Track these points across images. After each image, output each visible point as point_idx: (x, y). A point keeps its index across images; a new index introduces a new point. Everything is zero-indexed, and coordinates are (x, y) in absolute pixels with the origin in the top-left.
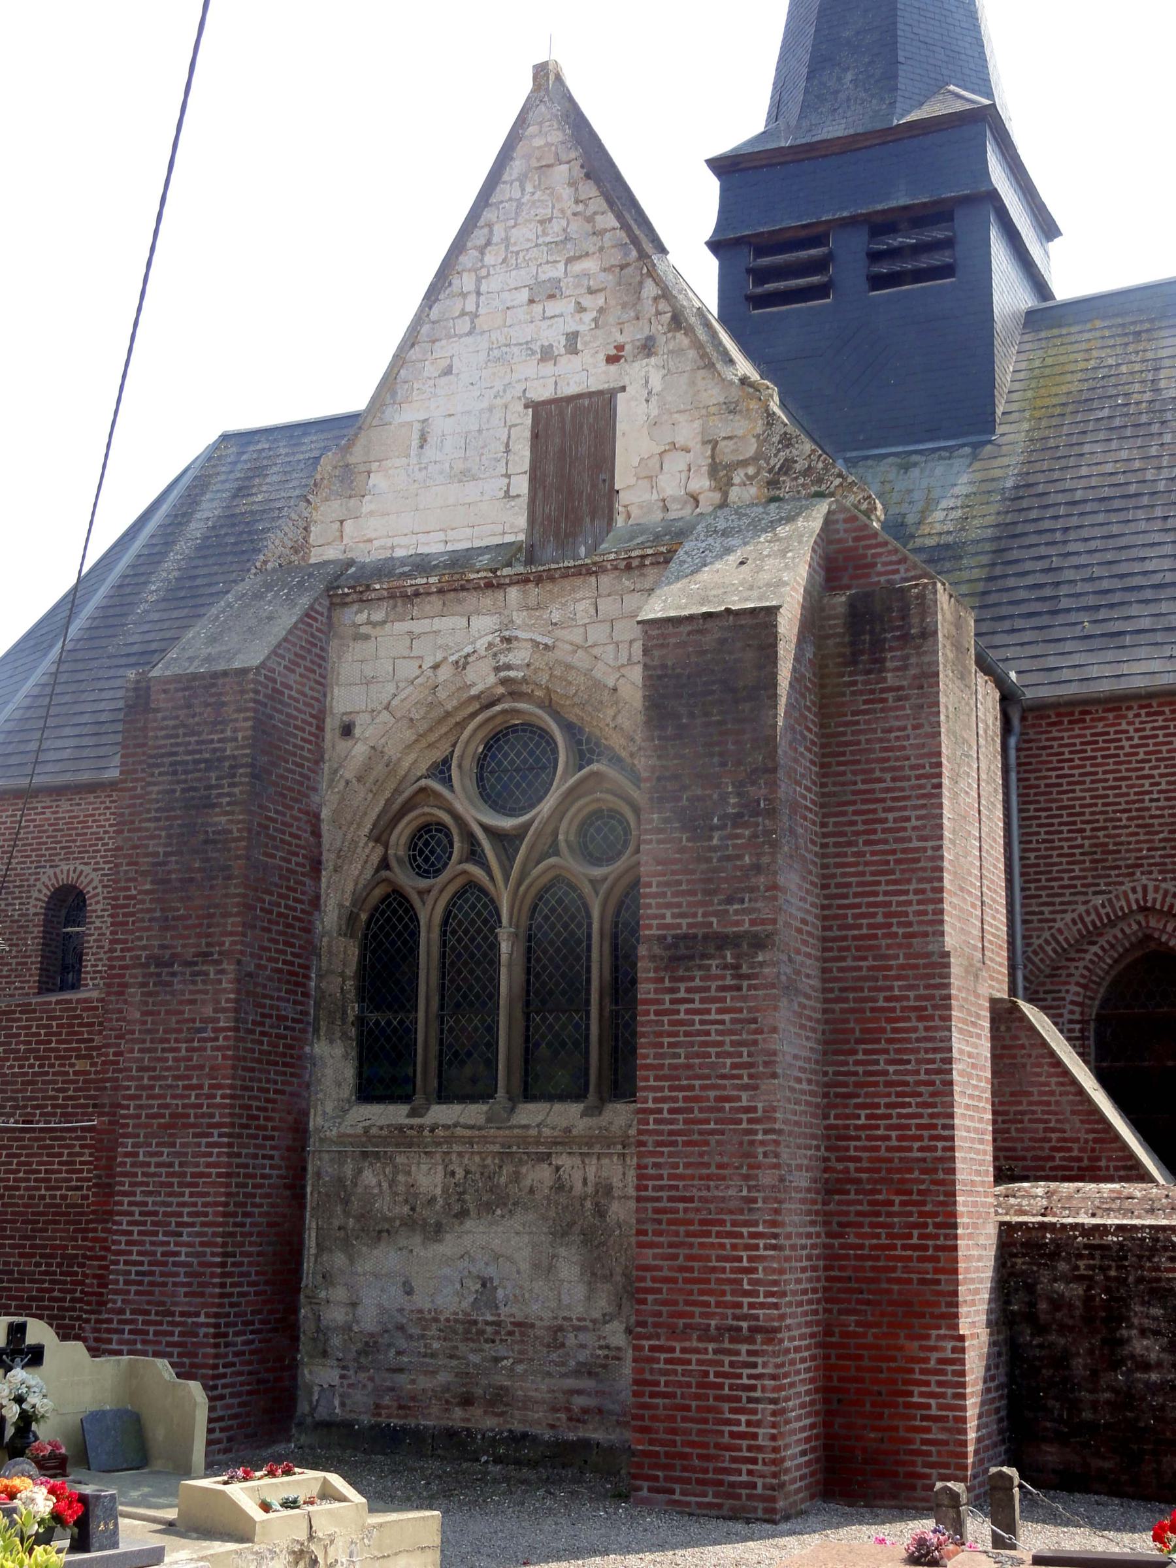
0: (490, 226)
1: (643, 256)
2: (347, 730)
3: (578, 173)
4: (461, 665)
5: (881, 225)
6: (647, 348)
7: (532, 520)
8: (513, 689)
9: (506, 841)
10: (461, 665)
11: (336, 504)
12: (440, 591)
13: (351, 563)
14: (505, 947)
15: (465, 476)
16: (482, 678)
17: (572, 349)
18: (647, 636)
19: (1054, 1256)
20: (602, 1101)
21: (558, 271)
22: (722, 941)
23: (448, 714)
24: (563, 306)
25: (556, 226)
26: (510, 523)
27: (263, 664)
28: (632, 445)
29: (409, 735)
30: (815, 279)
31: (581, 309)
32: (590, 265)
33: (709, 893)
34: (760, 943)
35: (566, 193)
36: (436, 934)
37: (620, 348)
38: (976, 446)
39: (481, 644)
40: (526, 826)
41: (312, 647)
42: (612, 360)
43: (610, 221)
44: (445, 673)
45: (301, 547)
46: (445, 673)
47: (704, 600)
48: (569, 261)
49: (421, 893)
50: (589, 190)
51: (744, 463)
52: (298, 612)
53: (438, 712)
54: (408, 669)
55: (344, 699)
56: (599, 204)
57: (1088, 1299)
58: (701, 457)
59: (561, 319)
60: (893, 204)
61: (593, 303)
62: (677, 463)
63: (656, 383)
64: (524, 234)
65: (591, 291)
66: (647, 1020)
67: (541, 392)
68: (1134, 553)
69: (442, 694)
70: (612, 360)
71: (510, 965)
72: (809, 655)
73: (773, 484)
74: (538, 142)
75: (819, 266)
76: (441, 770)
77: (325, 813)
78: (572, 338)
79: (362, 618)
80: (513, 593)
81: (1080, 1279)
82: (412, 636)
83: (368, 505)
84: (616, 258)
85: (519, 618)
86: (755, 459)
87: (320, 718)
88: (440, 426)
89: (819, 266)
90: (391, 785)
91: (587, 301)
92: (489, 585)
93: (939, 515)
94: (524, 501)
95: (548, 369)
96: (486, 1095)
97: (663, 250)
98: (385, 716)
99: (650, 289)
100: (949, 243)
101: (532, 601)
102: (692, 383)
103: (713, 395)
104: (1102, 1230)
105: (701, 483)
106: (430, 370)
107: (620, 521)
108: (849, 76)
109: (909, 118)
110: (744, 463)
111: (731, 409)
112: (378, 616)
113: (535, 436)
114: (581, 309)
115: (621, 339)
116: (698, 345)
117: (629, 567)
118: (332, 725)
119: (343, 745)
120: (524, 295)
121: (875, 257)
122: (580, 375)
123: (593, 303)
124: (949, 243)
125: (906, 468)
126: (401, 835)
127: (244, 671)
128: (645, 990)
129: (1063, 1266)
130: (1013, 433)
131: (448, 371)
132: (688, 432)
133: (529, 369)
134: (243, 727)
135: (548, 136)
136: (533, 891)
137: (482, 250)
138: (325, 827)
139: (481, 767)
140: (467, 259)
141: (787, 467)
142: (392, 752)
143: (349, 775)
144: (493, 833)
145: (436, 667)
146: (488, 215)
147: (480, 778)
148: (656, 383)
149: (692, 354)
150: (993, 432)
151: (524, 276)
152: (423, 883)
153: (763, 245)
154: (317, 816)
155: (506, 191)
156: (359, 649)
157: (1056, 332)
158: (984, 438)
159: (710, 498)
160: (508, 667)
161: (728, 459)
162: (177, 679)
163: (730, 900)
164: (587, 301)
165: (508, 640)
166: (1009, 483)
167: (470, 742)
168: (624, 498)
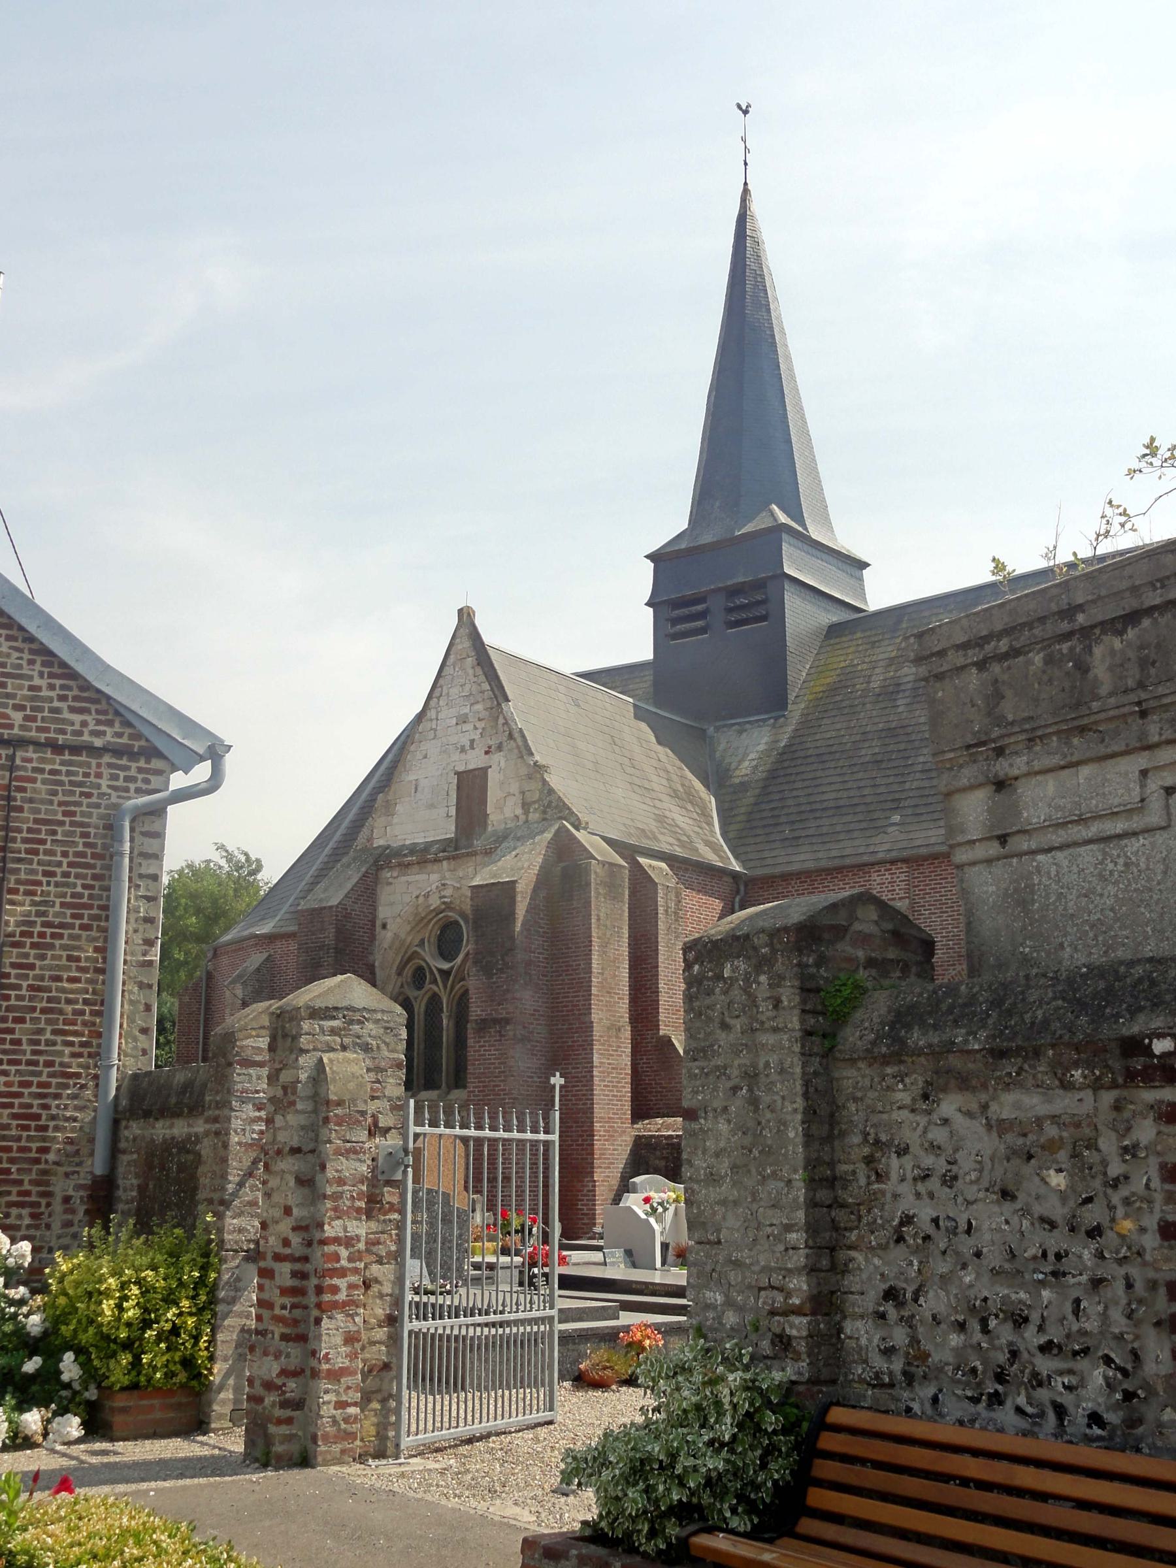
0: (441, 687)
1: (499, 704)
2: (384, 926)
3: (475, 662)
4: (427, 896)
5: (734, 591)
6: (500, 748)
7: (456, 827)
8: (448, 906)
9: (445, 974)
10: (427, 896)
11: (383, 819)
12: (418, 863)
13: (388, 847)
14: (445, 1022)
15: (432, 806)
16: (435, 902)
17: (472, 748)
18: (472, 893)
19: (655, 1149)
20: (449, 1089)
21: (466, 710)
22: (496, 1021)
23: (423, 918)
24: (468, 727)
25: (467, 687)
26: (448, 830)
27: (340, 903)
28: (494, 794)
29: (409, 928)
30: (700, 623)
31: (476, 728)
32: (479, 707)
33: (492, 1001)
34: (507, 1021)
35: (471, 672)
36: (422, 1016)
37: (490, 747)
38: (776, 719)
39: (434, 887)
40: (452, 967)
41: (368, 890)
42: (487, 753)
43: (486, 686)
44: (421, 899)
45: (370, 839)
46: (421, 899)
47: (495, 876)
48: (472, 705)
49: (416, 998)
50: (479, 671)
51: (534, 802)
52: (360, 875)
53: (418, 918)
54: (407, 899)
55: (383, 913)
56: (482, 678)
57: (666, 1167)
58: (518, 799)
59: (470, 732)
60: (735, 581)
61: (480, 725)
62: (511, 802)
63: (503, 764)
64: (454, 691)
65: (480, 720)
66: (471, 1054)
67: (461, 768)
68: (820, 789)
69: (420, 910)
70: (487, 753)
71: (448, 1030)
72: (542, 895)
73: (544, 812)
74: (460, 647)
75: (702, 615)
76: (421, 943)
77: (377, 964)
78: (472, 741)
79: (389, 875)
80: (445, 863)
81: (664, 1158)
82: (409, 883)
83: (396, 820)
84: (489, 705)
85: (447, 874)
86: (540, 799)
87: (373, 922)
88: (423, 783)
89: (702, 615)
90: (403, 950)
91: (478, 725)
92: (435, 860)
93: (746, 763)
94: (454, 818)
95: (463, 756)
96: (438, 1087)
97: (507, 700)
98: (398, 920)
99: (501, 721)
100: (763, 602)
101: (452, 867)
102: (516, 764)
103: (524, 771)
104: (671, 1137)
105: (519, 811)
106: (419, 756)
107: (490, 829)
108: (717, 504)
109: (743, 531)
110: (534, 802)
111: (530, 777)
112: (395, 874)
113: (458, 788)
114: (476, 728)
115: (491, 743)
116: (518, 747)
117: (486, 853)
118: (378, 923)
119: (383, 932)
120: (454, 721)
121: (730, 610)
122: (475, 760)
123: (480, 725)
124: (763, 602)
125: (740, 732)
126: (408, 971)
127: (331, 907)
128: (470, 1042)
129: (658, 1153)
130: (795, 711)
131: (425, 757)
132: (514, 788)
133: (456, 756)
134: (331, 932)
135: (465, 644)
136: (457, 997)
137: (438, 698)
138: (377, 971)
139: (439, 940)
140: (433, 703)
141: (549, 805)
142: (403, 936)
143: (386, 946)
144: (440, 971)
145: (417, 897)
146: (441, 681)
147: (439, 947)
148: (503, 764)
149: (516, 751)
150: (785, 709)
151: (453, 712)
152: (416, 993)
153: (676, 604)
154: (373, 966)
155: (448, 670)
156: (388, 889)
157: (837, 640)
158: (781, 713)
159: (522, 818)
160: (444, 897)
161: (529, 800)
162: (307, 910)
163: (499, 1004)
164: (478, 725)
165: (444, 885)
166: (782, 744)
167: (431, 931)
168: (491, 817)
